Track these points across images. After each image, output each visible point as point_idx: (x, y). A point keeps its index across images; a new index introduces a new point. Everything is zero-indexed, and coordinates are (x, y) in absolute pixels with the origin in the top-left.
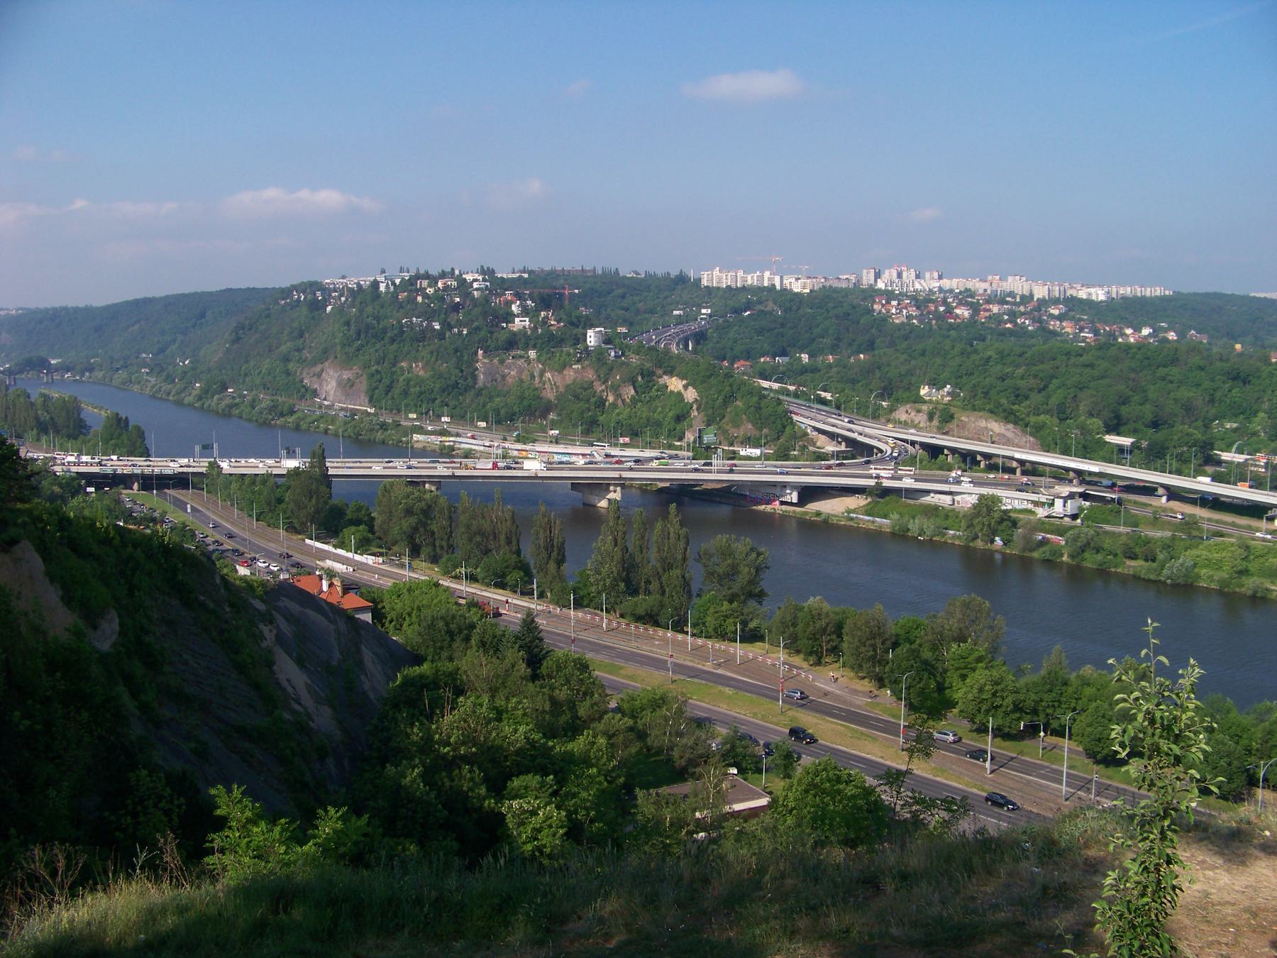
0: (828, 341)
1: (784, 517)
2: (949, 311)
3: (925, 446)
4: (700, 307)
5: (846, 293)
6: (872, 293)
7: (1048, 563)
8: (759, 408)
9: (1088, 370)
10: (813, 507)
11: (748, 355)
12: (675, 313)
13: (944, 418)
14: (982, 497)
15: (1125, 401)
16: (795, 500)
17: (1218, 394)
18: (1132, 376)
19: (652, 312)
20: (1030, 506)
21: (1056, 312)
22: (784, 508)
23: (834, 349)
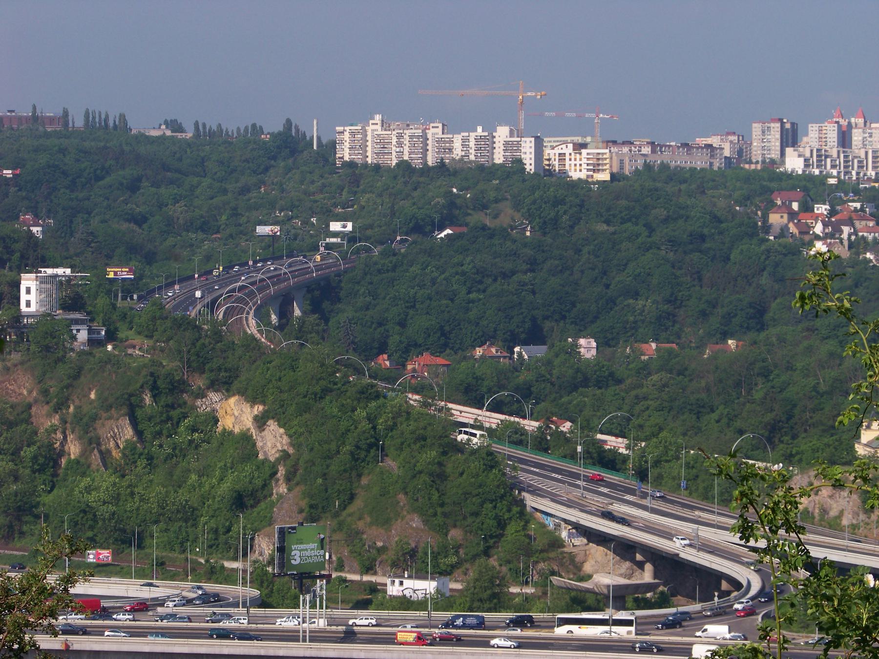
0: (647, 305)
5: (700, 181)
6: (770, 182)
8: (439, 477)
11: (445, 340)
12: (263, 230)
19: (206, 227)
23: (663, 325)
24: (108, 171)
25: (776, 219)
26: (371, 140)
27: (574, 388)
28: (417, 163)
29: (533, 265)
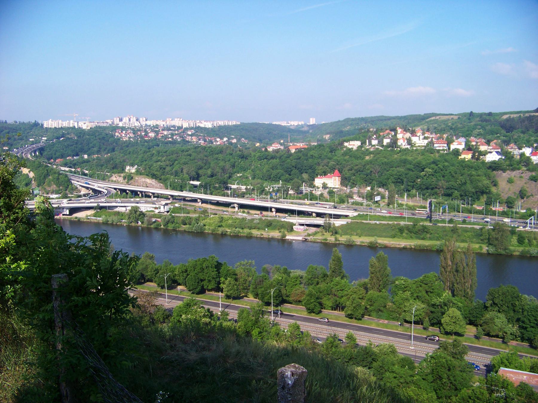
0: (95, 149)
1: (64, 220)
2: (146, 135)
3: (120, 190)
4: (42, 136)
5: (104, 128)
6: (115, 128)
7: (157, 229)
8: (58, 179)
9: (189, 157)
10: (75, 215)
11: (62, 156)
12: (31, 140)
13: (129, 178)
14: (132, 207)
15: (201, 168)
16: (68, 213)
17: (236, 163)
18: (205, 158)
19: (21, 139)
20: (153, 209)
21: (190, 133)
22: (64, 216)
23: (98, 152)
24: (3, 130)
25: (117, 134)
26: (49, 124)
27: (83, 163)
28: (58, 127)
29: (77, 143)
